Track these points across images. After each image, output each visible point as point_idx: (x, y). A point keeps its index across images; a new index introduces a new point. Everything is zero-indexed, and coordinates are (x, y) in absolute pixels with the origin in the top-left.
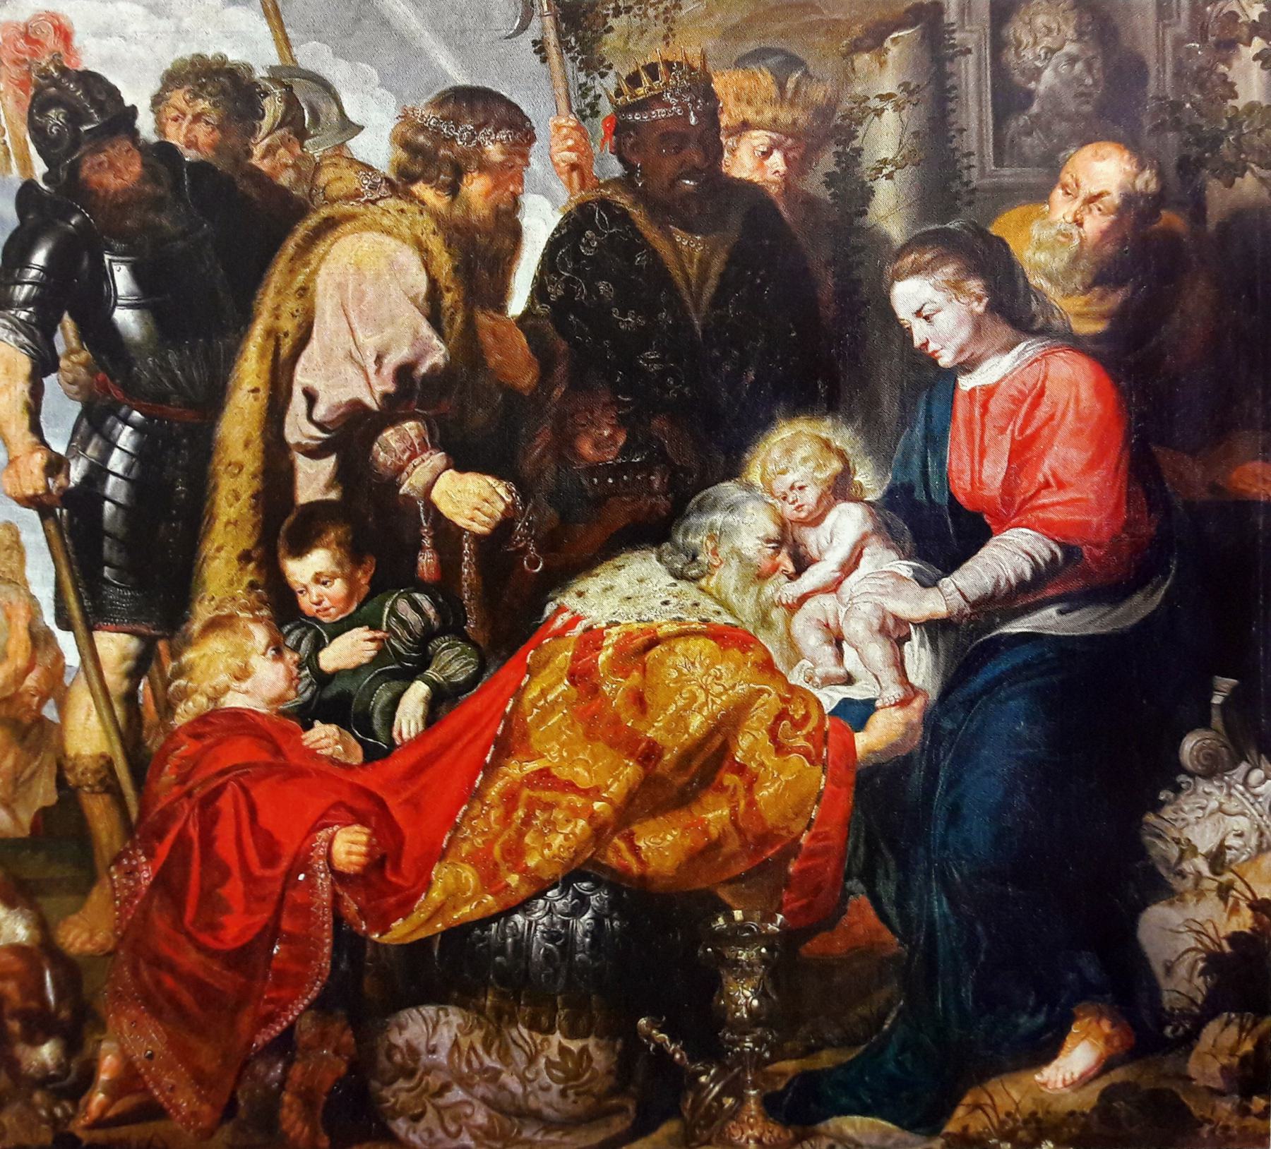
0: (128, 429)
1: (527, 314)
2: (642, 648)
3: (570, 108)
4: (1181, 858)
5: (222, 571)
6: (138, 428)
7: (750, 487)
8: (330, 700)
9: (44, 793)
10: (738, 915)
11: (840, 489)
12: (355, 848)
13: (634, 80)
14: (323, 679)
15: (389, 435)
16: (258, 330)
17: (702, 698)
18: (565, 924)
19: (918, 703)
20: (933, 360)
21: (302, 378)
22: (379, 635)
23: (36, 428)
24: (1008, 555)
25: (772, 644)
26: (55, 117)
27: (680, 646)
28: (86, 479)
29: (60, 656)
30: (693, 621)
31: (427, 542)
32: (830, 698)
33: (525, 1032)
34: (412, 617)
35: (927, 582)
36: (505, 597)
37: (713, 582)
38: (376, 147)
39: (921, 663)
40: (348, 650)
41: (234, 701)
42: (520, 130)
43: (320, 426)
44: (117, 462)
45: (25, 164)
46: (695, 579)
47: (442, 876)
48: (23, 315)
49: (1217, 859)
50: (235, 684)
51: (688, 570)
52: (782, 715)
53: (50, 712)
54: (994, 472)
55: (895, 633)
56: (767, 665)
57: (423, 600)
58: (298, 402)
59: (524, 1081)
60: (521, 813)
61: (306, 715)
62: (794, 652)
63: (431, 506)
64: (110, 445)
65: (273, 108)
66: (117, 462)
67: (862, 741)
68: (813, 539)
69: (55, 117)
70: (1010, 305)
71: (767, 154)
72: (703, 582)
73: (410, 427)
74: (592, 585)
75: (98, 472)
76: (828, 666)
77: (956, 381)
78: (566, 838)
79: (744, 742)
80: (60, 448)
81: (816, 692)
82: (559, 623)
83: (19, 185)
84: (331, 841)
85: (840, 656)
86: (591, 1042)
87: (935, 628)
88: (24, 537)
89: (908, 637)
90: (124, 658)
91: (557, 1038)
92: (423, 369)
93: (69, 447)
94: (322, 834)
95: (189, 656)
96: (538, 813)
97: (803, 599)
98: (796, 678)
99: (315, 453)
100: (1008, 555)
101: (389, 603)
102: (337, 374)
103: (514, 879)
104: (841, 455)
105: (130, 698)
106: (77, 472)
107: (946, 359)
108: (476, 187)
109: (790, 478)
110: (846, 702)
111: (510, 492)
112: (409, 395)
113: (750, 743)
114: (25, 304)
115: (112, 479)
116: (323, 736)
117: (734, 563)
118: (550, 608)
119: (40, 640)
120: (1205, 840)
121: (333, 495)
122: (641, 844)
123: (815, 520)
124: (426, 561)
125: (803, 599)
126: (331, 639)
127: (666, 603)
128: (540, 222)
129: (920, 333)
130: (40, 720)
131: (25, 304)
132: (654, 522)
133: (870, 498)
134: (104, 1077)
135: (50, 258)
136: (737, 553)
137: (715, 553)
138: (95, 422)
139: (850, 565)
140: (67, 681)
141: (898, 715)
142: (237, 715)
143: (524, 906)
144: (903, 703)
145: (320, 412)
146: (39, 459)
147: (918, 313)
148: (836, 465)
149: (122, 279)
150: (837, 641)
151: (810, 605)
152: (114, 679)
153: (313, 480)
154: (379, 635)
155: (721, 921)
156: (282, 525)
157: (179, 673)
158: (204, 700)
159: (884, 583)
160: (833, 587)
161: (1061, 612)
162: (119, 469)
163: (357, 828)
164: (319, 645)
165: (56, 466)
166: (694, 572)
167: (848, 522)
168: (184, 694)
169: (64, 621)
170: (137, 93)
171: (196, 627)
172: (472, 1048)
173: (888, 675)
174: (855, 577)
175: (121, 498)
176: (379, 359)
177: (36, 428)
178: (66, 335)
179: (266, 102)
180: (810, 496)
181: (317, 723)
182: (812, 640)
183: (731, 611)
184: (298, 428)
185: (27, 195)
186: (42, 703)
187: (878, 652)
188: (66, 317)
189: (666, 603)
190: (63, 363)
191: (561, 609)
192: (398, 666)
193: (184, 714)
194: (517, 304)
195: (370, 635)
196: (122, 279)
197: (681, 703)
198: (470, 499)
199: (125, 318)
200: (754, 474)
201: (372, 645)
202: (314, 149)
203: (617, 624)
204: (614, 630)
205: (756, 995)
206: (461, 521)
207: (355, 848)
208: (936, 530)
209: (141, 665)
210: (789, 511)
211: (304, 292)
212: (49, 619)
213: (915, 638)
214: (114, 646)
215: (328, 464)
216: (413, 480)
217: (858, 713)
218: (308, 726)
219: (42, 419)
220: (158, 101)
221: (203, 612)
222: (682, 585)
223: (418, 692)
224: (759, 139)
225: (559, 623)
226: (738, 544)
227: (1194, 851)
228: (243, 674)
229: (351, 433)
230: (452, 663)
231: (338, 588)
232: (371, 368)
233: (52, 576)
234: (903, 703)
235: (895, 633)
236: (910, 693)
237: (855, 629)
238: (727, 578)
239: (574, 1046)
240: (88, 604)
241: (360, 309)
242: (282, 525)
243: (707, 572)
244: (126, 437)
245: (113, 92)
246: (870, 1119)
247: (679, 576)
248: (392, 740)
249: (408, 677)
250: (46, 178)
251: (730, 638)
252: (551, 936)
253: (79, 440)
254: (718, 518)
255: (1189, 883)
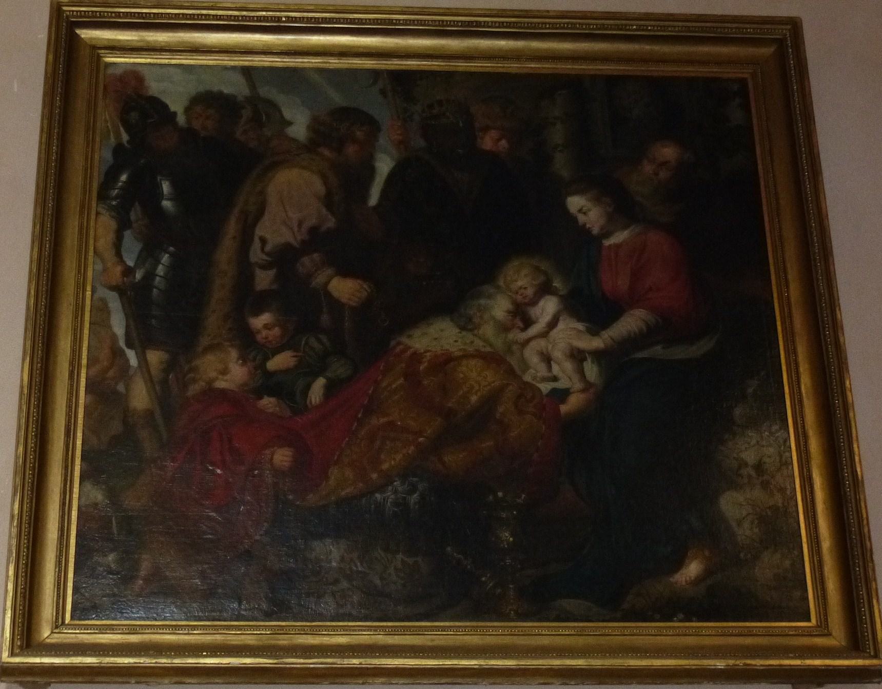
0: (167, 256)
1: (379, 205)
2: (444, 363)
3: (399, 117)
4: (740, 467)
5: (214, 320)
6: (172, 255)
7: (498, 287)
8: (270, 384)
9: (116, 427)
10: (500, 494)
11: (545, 289)
12: (285, 458)
13: (431, 106)
14: (269, 375)
15: (306, 260)
16: (236, 211)
17: (477, 388)
18: (404, 498)
19: (592, 390)
20: (588, 232)
21: (259, 232)
22: (300, 354)
23: (119, 254)
24: (630, 323)
25: (513, 361)
26: (134, 116)
27: (464, 362)
28: (144, 278)
29: (127, 361)
30: (471, 349)
31: (325, 310)
32: (545, 387)
33: (383, 554)
34: (316, 345)
35: (594, 332)
36: (369, 338)
37: (481, 332)
38: (299, 129)
39: (591, 370)
40: (281, 361)
41: (221, 384)
42: (373, 126)
43: (268, 254)
44: (160, 270)
45: (118, 135)
46: (471, 330)
47: (334, 473)
48: (114, 203)
49: (759, 467)
50: (220, 377)
51: (467, 325)
52: (520, 396)
53: (121, 388)
54: (623, 283)
55: (578, 356)
56: (511, 372)
57: (324, 339)
58: (257, 244)
59: (382, 579)
60: (378, 443)
61: (259, 393)
62: (526, 366)
63: (328, 295)
64: (158, 262)
65: (247, 113)
66: (160, 270)
67: (564, 408)
68: (534, 312)
69: (134, 116)
70: (623, 209)
71: (499, 140)
72: (476, 332)
73: (316, 256)
74: (417, 332)
75: (150, 276)
76: (542, 370)
77: (601, 243)
78: (404, 455)
79: (501, 409)
80: (131, 263)
81: (538, 385)
82: (398, 350)
83: (114, 145)
84: (273, 454)
85: (550, 368)
86: (419, 559)
87: (598, 355)
88: (110, 305)
89: (585, 359)
90: (161, 362)
91: (400, 556)
92: (324, 229)
93: (136, 263)
94: (267, 452)
95: (197, 362)
96: (388, 443)
97: (528, 341)
98: (527, 378)
99: (265, 267)
100: (630, 323)
101: (304, 339)
102: (275, 230)
103: (374, 476)
104: (545, 273)
105: (164, 382)
106: (139, 275)
107: (596, 231)
108: (351, 150)
109: (520, 283)
110: (554, 391)
111: (370, 287)
112: (315, 239)
113: (504, 408)
114: (116, 198)
115: (158, 278)
116: (268, 403)
117: (491, 323)
118: (393, 343)
119: (117, 353)
120: (750, 457)
121: (274, 287)
122: (446, 459)
123: (534, 302)
124: (325, 319)
125: (528, 341)
126: (273, 356)
127: (456, 341)
128: (384, 166)
129: (581, 218)
130: (115, 392)
131: (116, 198)
132: (452, 303)
133: (561, 293)
134: (143, 573)
135: (129, 178)
136: (493, 318)
137: (481, 317)
138: (149, 252)
139: (553, 324)
140: (131, 372)
141: (582, 396)
142: (223, 392)
143: (381, 488)
144: (583, 391)
145: (268, 248)
146: (119, 269)
147: (580, 211)
148: (542, 278)
149: (166, 187)
150: (547, 359)
151: (533, 344)
152: (154, 371)
153: (264, 280)
154: (300, 354)
155: (491, 497)
156: (246, 299)
157: (192, 370)
158: (204, 384)
159: (570, 334)
160: (544, 335)
161: (663, 348)
162: (162, 274)
163: (286, 448)
164: (266, 359)
165: (128, 272)
166: (470, 327)
167: (549, 307)
168: (194, 381)
169: (130, 345)
170: (177, 106)
171: (200, 349)
172: (352, 560)
173: (576, 378)
174: (555, 331)
175: (162, 287)
176: (300, 224)
177: (119, 254)
178: (135, 214)
179: (243, 112)
180: (530, 292)
181: (265, 397)
182: (534, 360)
183: (491, 345)
184: (256, 255)
185: (118, 150)
186: (116, 384)
187: (569, 366)
188: (137, 204)
189: (456, 341)
190: (134, 225)
191: (399, 343)
192: (308, 369)
193: (194, 389)
194: (373, 200)
195: (293, 354)
196: (166, 187)
197: (465, 389)
198: (345, 289)
199: (166, 204)
200: (501, 283)
201: (295, 359)
202: (267, 132)
203: (429, 351)
204: (428, 354)
205: (512, 535)
206: (344, 300)
207: (285, 458)
208: (593, 309)
209: (170, 366)
210: (519, 298)
211: (262, 193)
212: (122, 343)
213: (589, 360)
214: (155, 357)
215: (272, 273)
216: (318, 280)
217: (562, 395)
218: (261, 398)
219: (122, 250)
220: (187, 110)
221: (205, 341)
222: (464, 333)
223: (320, 382)
224: (494, 134)
225: (398, 350)
226: (493, 313)
227: (746, 465)
228: (225, 372)
229: (284, 258)
230: (339, 369)
231: (277, 331)
232: (296, 229)
233: (124, 323)
234: (583, 391)
235: (578, 356)
236: (588, 386)
237: (557, 354)
238: (488, 330)
239: (410, 561)
240: (142, 337)
241: (291, 201)
242: (246, 299)
243: (478, 327)
244: (165, 258)
245: (165, 107)
246: (579, 601)
247: (463, 328)
248: (307, 406)
249: (316, 376)
250: (128, 142)
251: (492, 359)
252: (396, 504)
253: (141, 260)
254: (482, 302)
255: (746, 480)
